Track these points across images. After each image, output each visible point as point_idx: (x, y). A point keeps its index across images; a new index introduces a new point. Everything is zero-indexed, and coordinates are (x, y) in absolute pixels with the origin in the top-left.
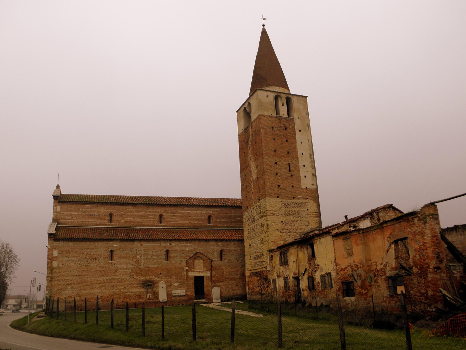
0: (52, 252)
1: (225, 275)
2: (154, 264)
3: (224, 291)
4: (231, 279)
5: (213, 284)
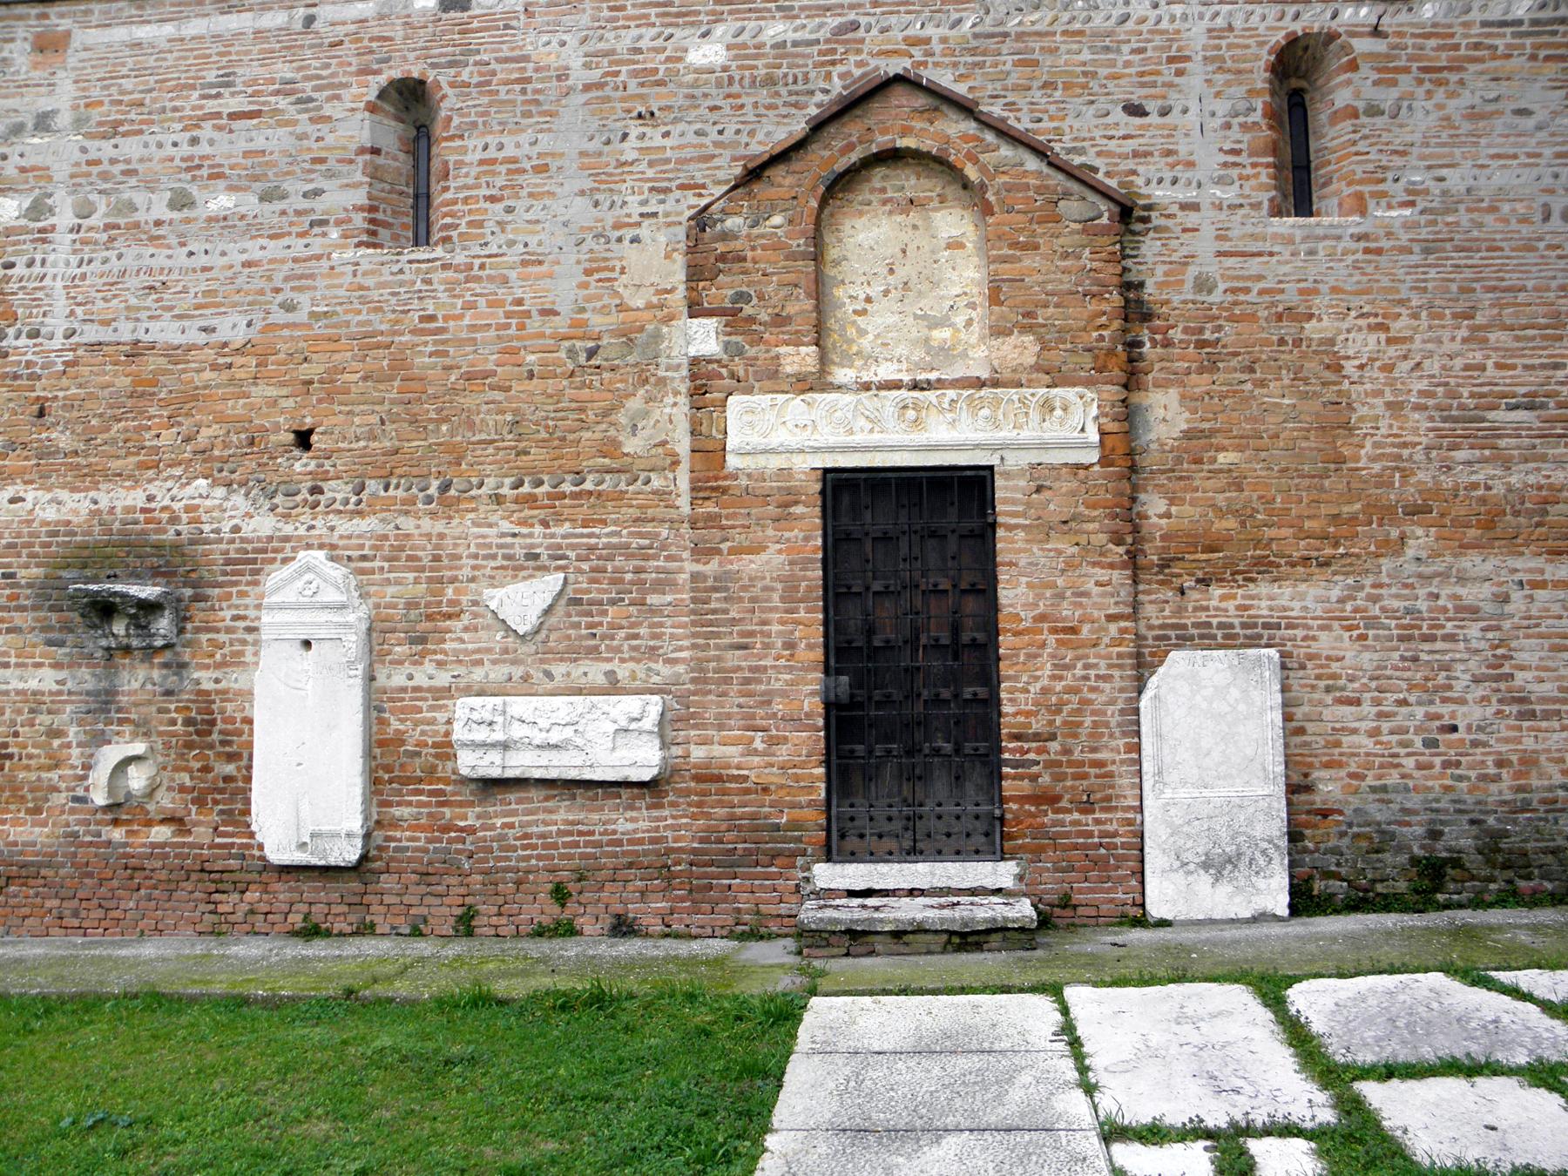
0: (852, 696)
1: (1366, 458)
2: (209, 302)
3: (1358, 731)
4: (1492, 525)
5: (1158, 608)
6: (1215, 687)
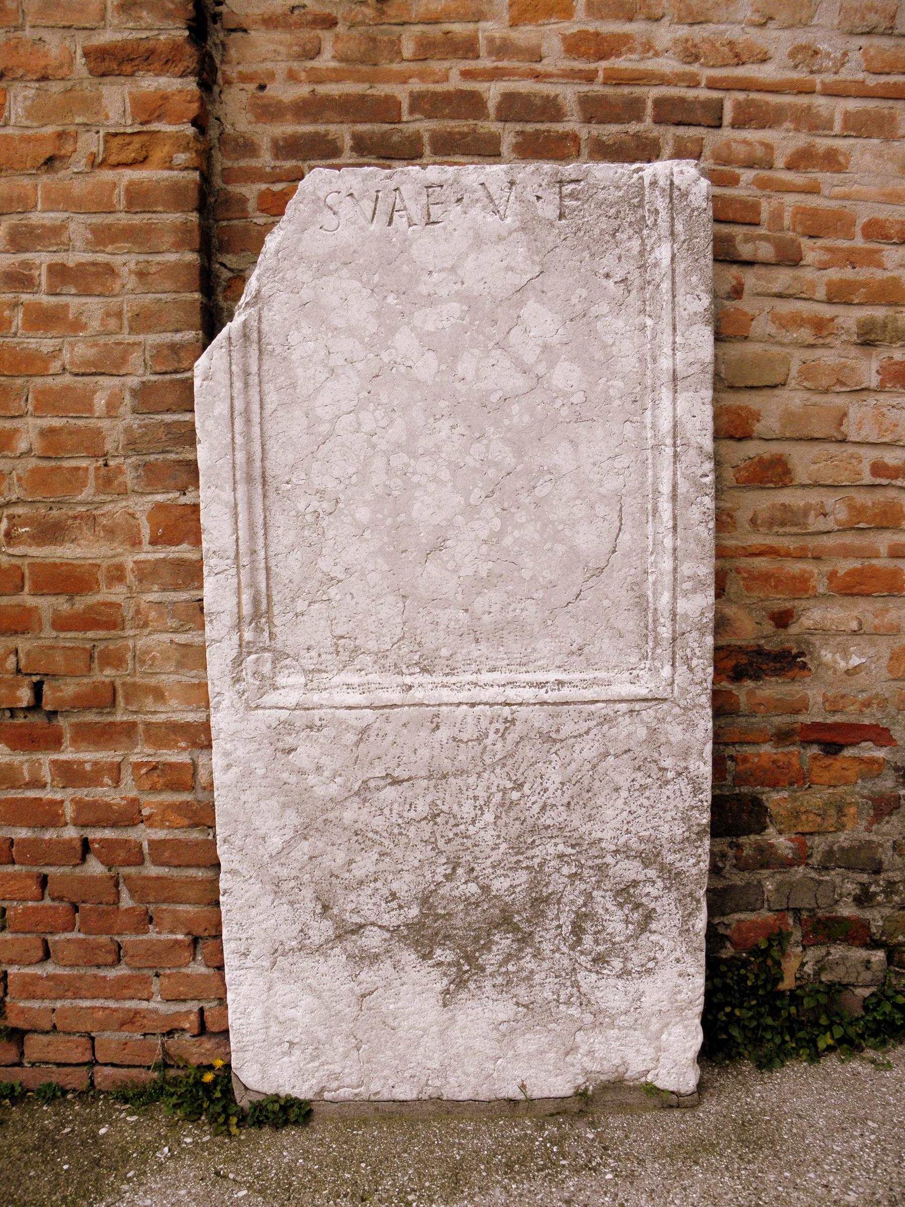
6: (470, 302)
